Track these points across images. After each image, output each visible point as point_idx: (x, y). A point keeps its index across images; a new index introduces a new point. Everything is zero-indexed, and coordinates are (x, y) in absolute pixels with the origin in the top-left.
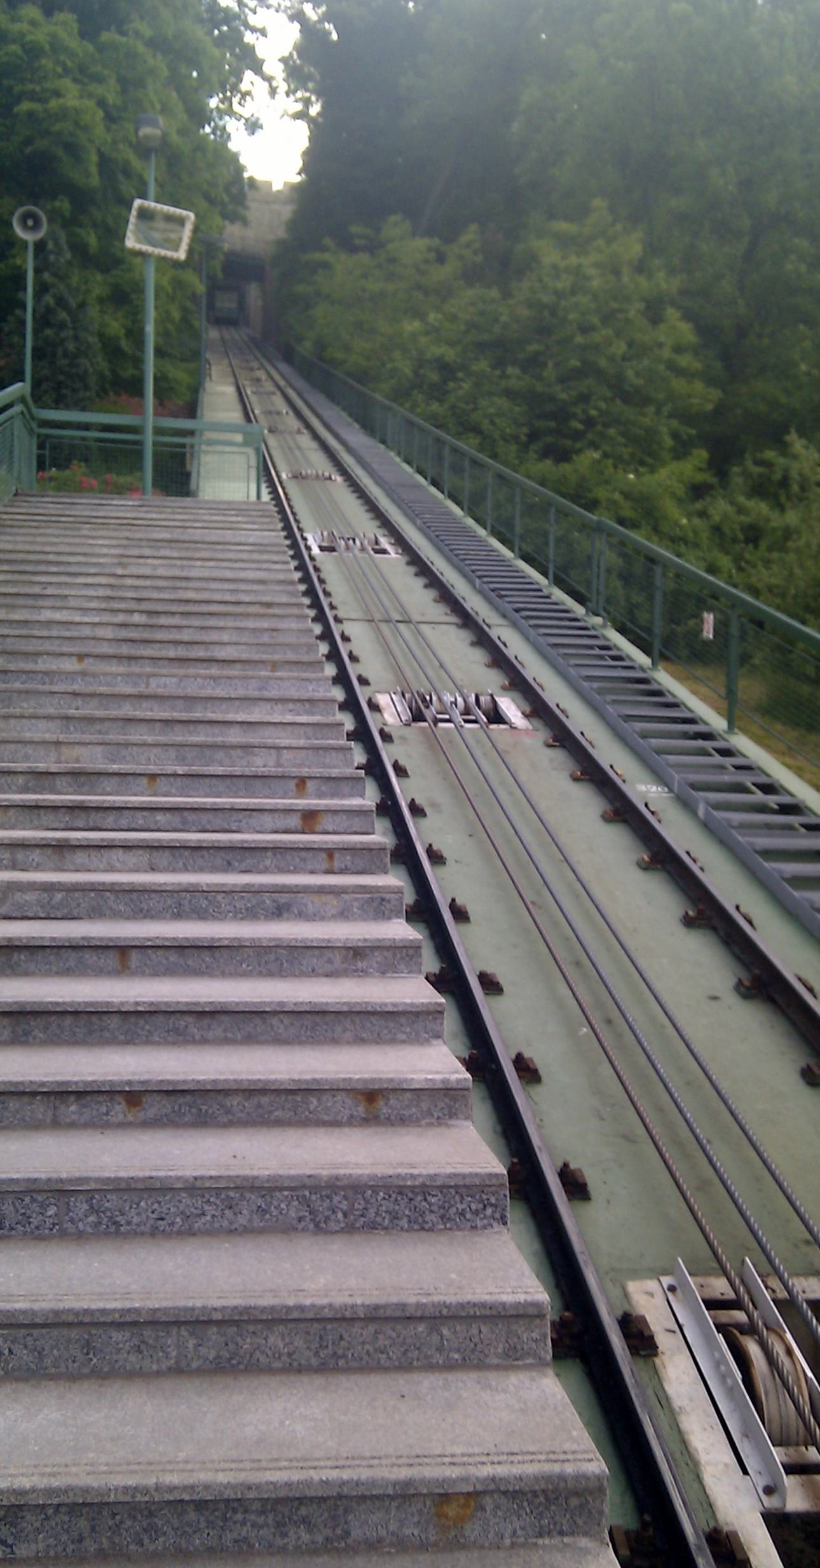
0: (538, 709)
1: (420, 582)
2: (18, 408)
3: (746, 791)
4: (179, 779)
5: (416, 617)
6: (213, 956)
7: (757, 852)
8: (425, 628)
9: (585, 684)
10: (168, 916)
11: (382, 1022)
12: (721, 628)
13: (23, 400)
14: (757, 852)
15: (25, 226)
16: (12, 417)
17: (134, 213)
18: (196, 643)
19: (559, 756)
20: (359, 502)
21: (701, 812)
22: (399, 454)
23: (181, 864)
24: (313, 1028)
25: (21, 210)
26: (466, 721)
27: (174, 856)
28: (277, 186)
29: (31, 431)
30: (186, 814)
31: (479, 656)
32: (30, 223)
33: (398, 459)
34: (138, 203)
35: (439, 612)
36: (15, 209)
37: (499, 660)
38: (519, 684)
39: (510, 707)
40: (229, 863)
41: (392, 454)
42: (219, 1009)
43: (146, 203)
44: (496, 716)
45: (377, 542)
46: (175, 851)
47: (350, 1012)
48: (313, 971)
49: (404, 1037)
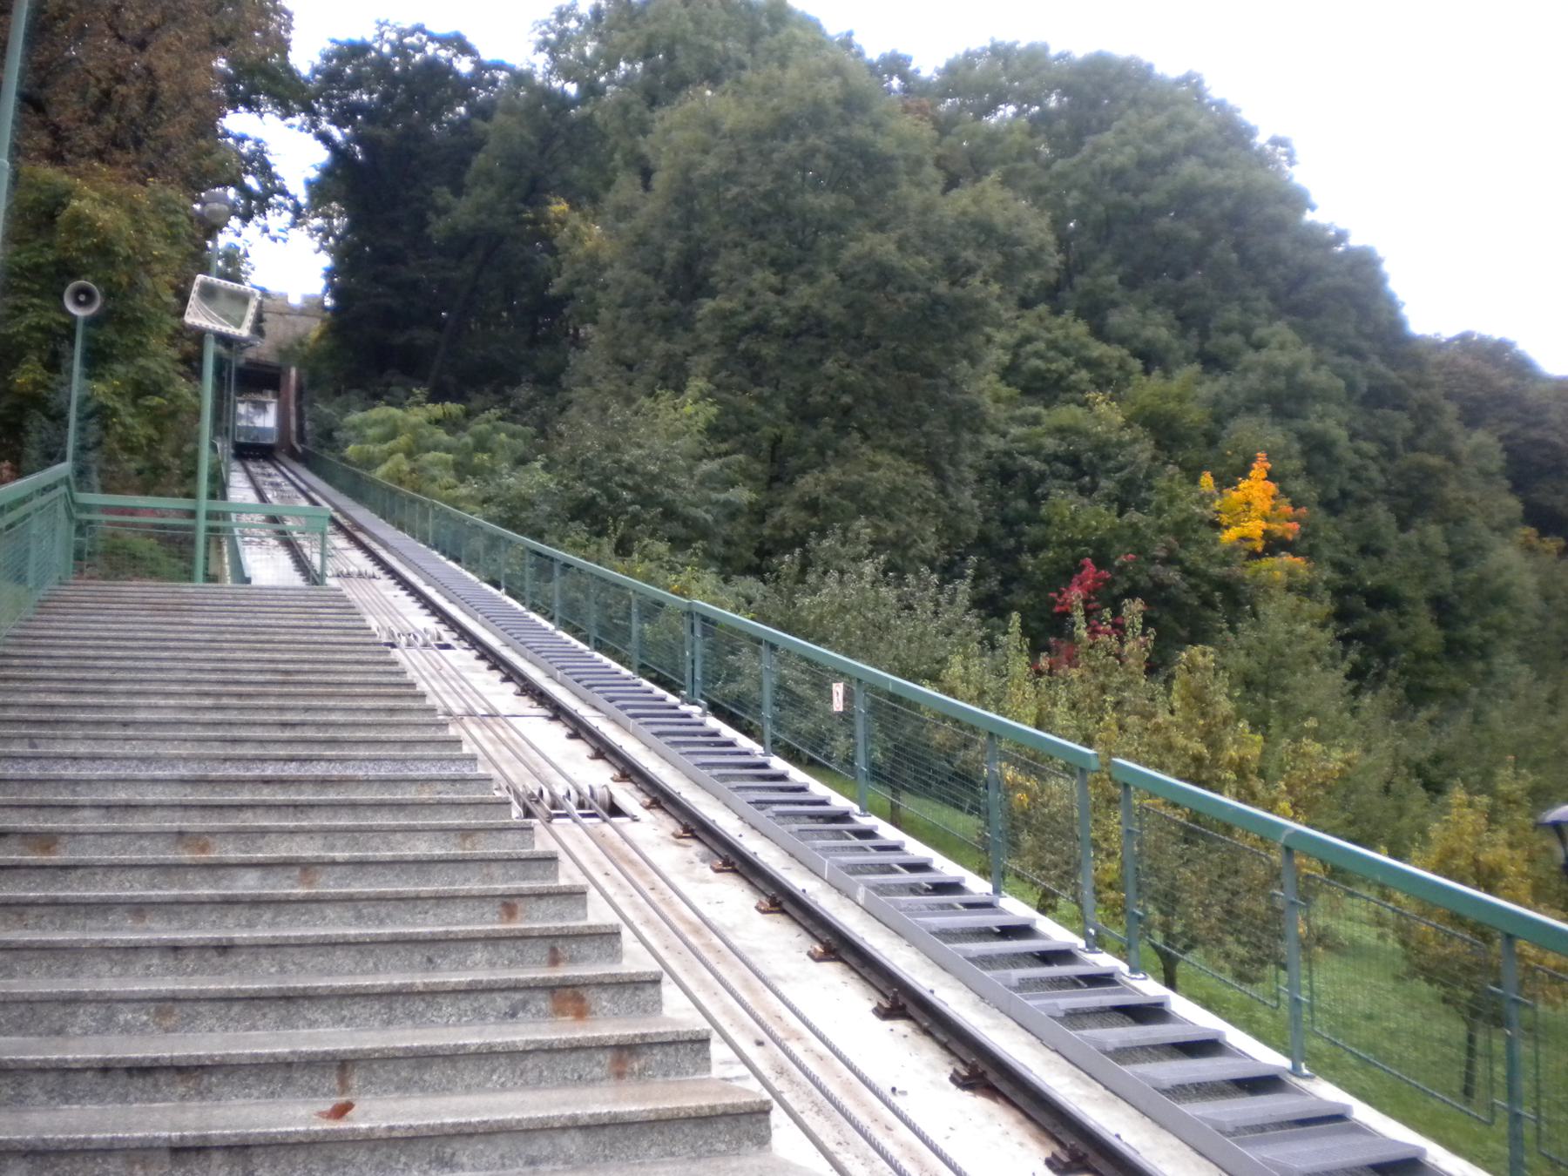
0: (661, 799)
1: (496, 676)
2: (63, 489)
3: (892, 871)
4: (337, 869)
5: (503, 712)
6: (454, 1067)
7: (934, 933)
8: (512, 720)
9: (705, 772)
10: (376, 1024)
11: (695, 1131)
12: (848, 697)
13: (66, 481)
14: (934, 933)
15: (78, 303)
16: (28, 515)
17: (195, 288)
18: (135, 807)
19: (695, 848)
20: (411, 599)
21: (860, 898)
22: (443, 553)
23: (371, 965)
24: (612, 1145)
25: (73, 285)
26: (584, 816)
27: (361, 953)
28: (295, 300)
29: (70, 518)
30: (360, 905)
31: (581, 749)
32: (82, 298)
33: (443, 558)
34: (200, 278)
35: (525, 705)
36: (64, 285)
37: (604, 751)
38: (630, 772)
39: (627, 796)
40: (430, 960)
41: (435, 553)
42: (495, 1128)
43: (209, 278)
44: (615, 810)
45: (439, 638)
46: (363, 948)
47: (659, 1121)
48: (580, 1077)
49: (723, 1147)
